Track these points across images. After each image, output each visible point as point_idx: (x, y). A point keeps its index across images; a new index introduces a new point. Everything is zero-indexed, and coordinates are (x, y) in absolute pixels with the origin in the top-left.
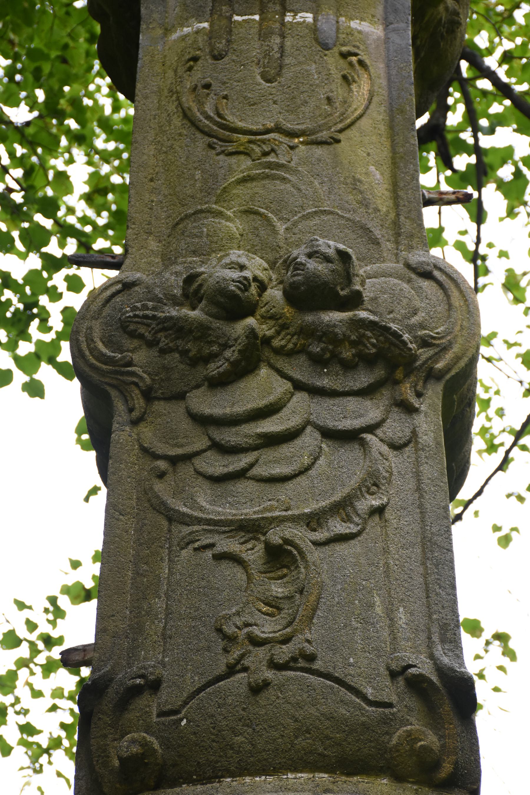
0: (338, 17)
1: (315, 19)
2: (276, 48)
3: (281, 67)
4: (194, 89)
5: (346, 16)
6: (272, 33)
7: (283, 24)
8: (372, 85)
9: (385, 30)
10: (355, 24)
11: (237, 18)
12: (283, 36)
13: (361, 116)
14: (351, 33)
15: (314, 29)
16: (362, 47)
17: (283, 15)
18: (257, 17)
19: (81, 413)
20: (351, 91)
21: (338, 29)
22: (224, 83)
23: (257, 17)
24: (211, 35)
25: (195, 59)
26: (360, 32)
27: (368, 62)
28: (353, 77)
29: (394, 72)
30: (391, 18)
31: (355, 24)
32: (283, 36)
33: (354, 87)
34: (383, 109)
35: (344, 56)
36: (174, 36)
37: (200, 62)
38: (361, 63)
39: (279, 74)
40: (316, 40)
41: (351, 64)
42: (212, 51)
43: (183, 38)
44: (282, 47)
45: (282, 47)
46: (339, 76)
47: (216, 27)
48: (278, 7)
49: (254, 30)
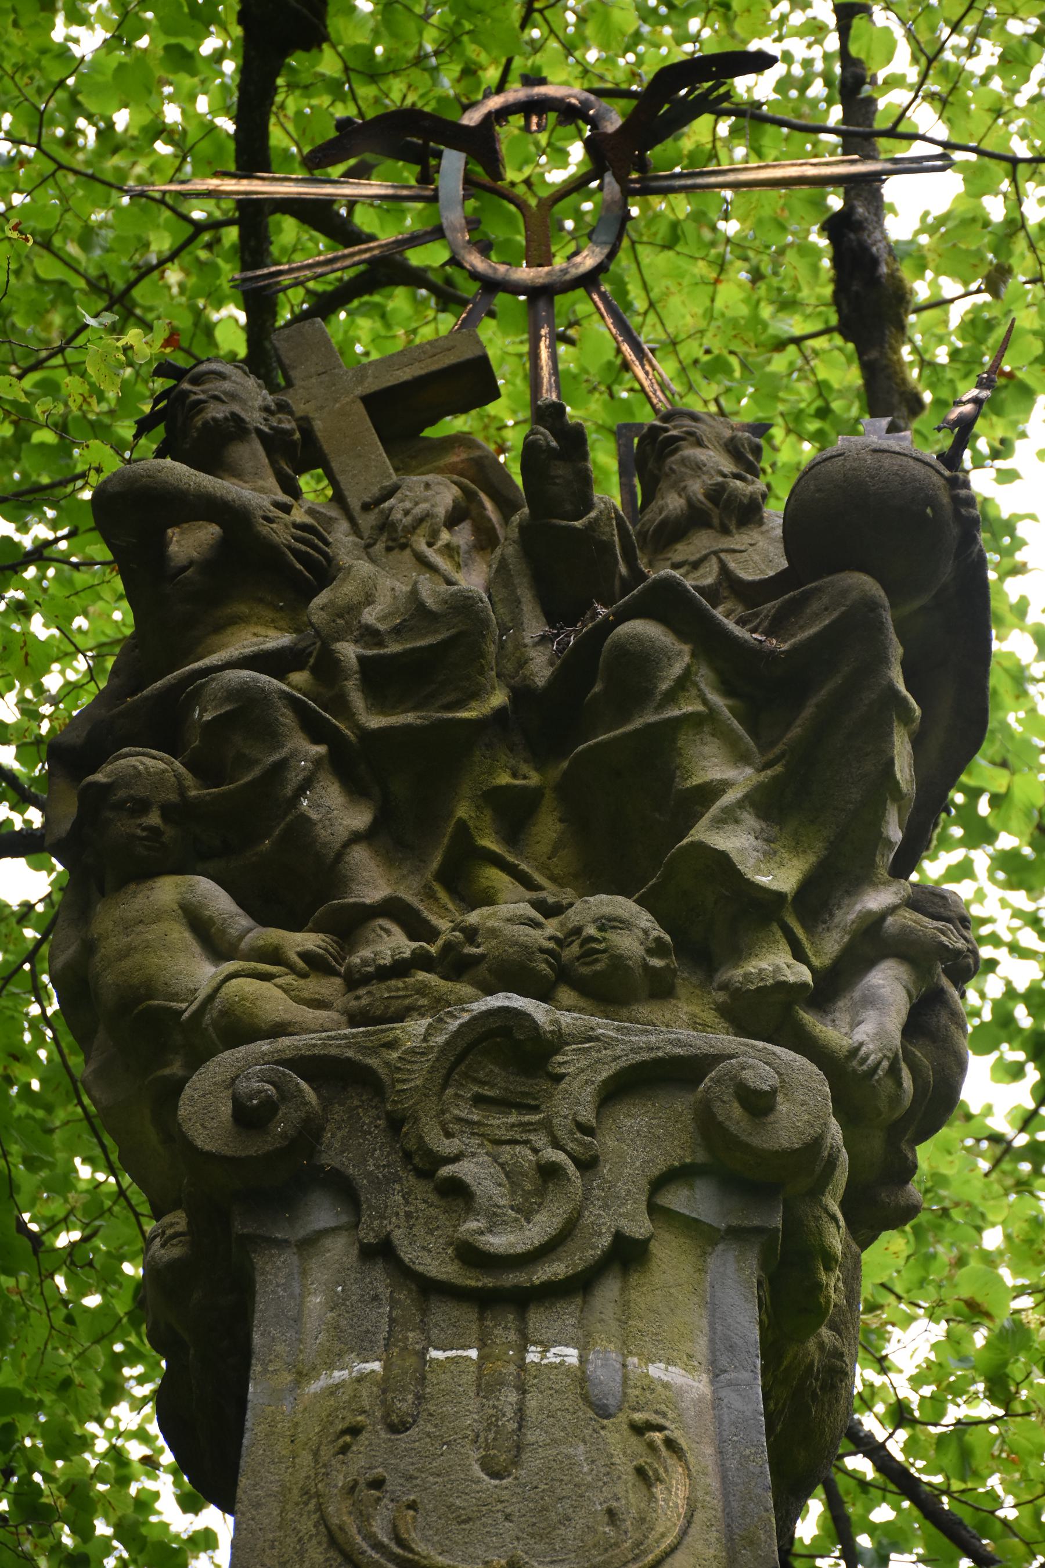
1: (582, 1359)
2: (510, 1414)
3: (519, 1448)
5: (640, 1355)
6: (502, 1384)
7: (522, 1366)
8: (693, 1488)
9: (712, 1382)
10: (656, 1370)
11: (434, 1354)
12: (522, 1390)
13: (673, 1549)
14: (649, 1386)
15: (581, 1378)
16: (671, 1415)
18: (473, 1353)
20: (652, 1497)
21: (625, 1378)
23: (473, 1353)
24: (386, 1384)
25: (355, 1431)
26: (666, 1386)
27: (683, 1443)
28: (655, 1471)
29: (732, 1464)
30: (724, 1361)
31: (656, 1370)
32: (522, 1390)
33: (658, 1490)
34: (713, 1535)
35: (639, 1429)
36: (315, 1387)
37: (363, 1437)
38: (670, 1443)
39: (516, 1462)
40: (585, 1398)
41: (651, 1446)
42: (387, 1415)
44: (520, 1411)
45: (520, 1411)
46: (630, 1469)
48: (513, 1336)
49: (469, 1378)
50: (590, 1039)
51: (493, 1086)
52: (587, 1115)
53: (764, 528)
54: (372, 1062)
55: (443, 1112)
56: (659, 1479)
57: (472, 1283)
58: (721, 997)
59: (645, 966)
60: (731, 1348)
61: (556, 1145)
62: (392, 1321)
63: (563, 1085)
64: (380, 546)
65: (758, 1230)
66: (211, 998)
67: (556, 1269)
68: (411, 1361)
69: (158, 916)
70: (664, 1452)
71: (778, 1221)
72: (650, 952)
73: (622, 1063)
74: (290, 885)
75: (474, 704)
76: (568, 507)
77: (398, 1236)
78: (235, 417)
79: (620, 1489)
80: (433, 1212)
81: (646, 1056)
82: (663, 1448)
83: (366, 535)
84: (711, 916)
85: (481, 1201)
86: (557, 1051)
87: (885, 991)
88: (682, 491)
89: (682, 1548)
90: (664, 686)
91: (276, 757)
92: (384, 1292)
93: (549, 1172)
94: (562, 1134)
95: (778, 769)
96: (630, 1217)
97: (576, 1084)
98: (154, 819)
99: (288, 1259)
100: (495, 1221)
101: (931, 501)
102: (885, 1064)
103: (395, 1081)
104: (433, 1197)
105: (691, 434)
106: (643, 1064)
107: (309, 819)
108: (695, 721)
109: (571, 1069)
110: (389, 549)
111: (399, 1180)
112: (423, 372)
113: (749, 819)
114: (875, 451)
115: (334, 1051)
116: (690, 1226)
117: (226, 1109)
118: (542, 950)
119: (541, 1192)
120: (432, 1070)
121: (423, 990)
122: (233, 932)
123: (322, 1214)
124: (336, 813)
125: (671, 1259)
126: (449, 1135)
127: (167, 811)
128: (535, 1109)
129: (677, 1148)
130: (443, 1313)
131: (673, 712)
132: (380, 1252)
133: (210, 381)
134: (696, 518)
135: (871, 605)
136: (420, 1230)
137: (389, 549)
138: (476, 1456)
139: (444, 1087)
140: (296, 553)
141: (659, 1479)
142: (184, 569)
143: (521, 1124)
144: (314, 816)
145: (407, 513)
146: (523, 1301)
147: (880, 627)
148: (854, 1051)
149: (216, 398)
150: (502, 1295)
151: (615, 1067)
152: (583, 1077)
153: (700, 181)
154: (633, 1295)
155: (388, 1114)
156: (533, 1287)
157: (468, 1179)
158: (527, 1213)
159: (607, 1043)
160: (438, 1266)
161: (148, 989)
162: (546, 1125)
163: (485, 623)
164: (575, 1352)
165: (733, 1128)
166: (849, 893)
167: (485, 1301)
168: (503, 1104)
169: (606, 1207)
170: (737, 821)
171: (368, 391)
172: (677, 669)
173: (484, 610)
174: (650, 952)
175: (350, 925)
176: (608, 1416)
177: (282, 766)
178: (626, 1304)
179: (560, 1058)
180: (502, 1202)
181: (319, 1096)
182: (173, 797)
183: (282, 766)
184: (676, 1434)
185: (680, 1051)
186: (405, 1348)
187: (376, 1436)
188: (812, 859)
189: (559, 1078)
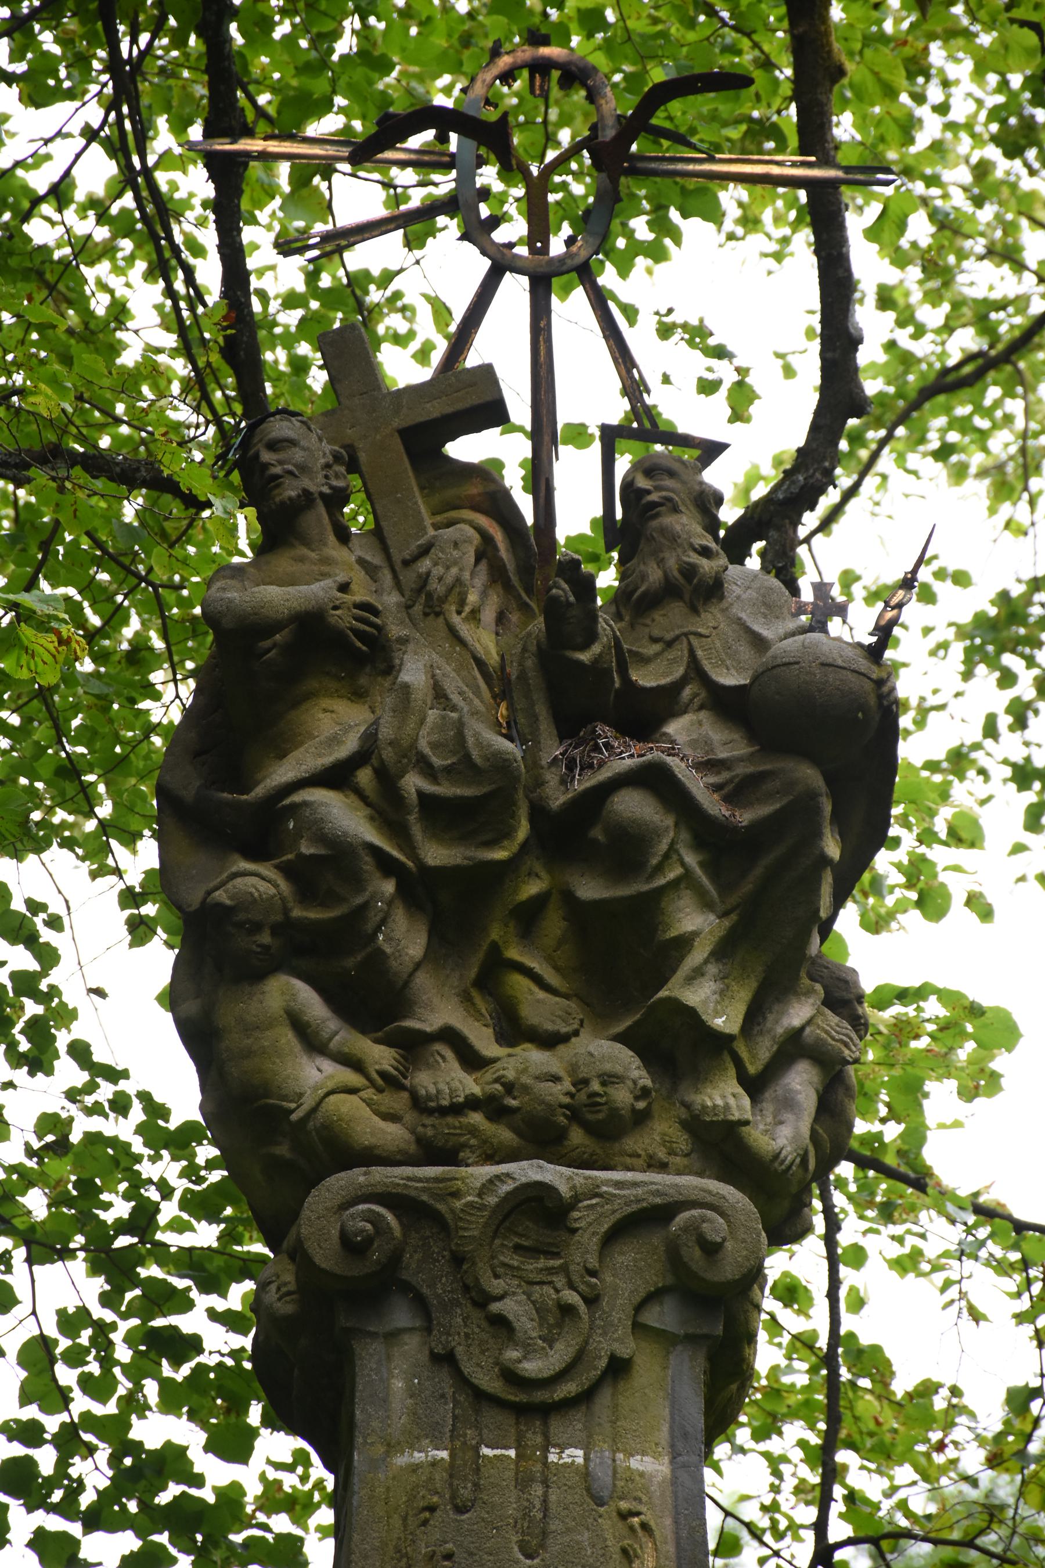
0: (614, 1452)
1: (587, 1458)
3: (545, 1534)
5: (624, 1451)
6: (532, 1480)
11: (486, 1451)
12: (546, 1483)
14: (631, 1476)
15: (586, 1473)
16: (644, 1498)
17: (546, 1451)
18: (512, 1453)
19: (168, 980)
21: (615, 1472)
22: (471, 1554)
23: (512, 1453)
24: (452, 1469)
25: (432, 1509)
26: (642, 1475)
27: (652, 1523)
29: (684, 1534)
30: (680, 1445)
32: (546, 1483)
35: (624, 1516)
36: (401, 1460)
37: (438, 1513)
38: (644, 1526)
39: (542, 1546)
40: (588, 1490)
41: (632, 1528)
42: (453, 1497)
43: (415, 1468)
44: (545, 1501)
45: (545, 1501)
47: (459, 1462)
48: (539, 1439)
49: (510, 1474)
51: (528, 1238)
52: (593, 1262)
53: (724, 604)
54: (441, 1207)
55: (493, 1258)
56: (637, 1557)
57: (512, 1398)
58: (683, 1114)
59: (633, 1110)
60: (685, 1435)
61: (572, 1286)
62: (455, 1417)
63: (577, 1237)
64: (418, 608)
65: (706, 1337)
66: (314, 1110)
68: (470, 1454)
70: (640, 1532)
71: (719, 1330)
72: (637, 1098)
73: (618, 1216)
74: (371, 1000)
75: (506, 843)
77: (460, 1350)
80: (484, 1336)
81: (635, 1207)
83: (408, 593)
84: (679, 1048)
87: (801, 1098)
88: (661, 562)
90: (654, 861)
91: (359, 900)
92: (449, 1391)
93: (567, 1310)
94: (576, 1278)
95: (734, 917)
97: (586, 1236)
98: (266, 938)
99: (376, 1347)
103: (458, 1228)
104: (484, 1324)
105: (669, 500)
106: (633, 1214)
107: (383, 952)
108: (675, 884)
109: (582, 1224)
110: (426, 615)
111: (459, 1305)
112: (449, 410)
113: (712, 969)
114: (823, 664)
115: (413, 1193)
118: (561, 1106)
119: (559, 1325)
120: (486, 1225)
121: (473, 1131)
122: (325, 1035)
123: (401, 1316)
124: (406, 940)
125: (647, 1368)
126: (497, 1276)
127: (276, 930)
128: (556, 1255)
129: (654, 1278)
130: (492, 1417)
131: (661, 881)
132: (445, 1359)
133: (283, 449)
134: (669, 591)
135: (812, 796)
138: (514, 1539)
139: (494, 1238)
140: (357, 633)
141: (637, 1557)
144: (388, 950)
145: (440, 579)
146: (546, 1411)
147: (818, 810)
148: (777, 1156)
149: (290, 473)
150: (534, 1409)
151: (613, 1219)
152: (591, 1230)
153: (680, 166)
155: (451, 1251)
157: (511, 1317)
158: (550, 1341)
160: (489, 1382)
161: (265, 1089)
162: (564, 1269)
163: (517, 779)
164: (580, 1453)
165: (694, 1267)
166: (778, 1000)
167: (521, 1411)
168: (534, 1252)
169: (605, 1334)
171: (405, 424)
172: (664, 846)
173: (518, 768)
174: (637, 1098)
175: (413, 1047)
176: (602, 1505)
177: (364, 907)
178: (616, 1406)
179: (576, 1214)
180: (534, 1334)
181: (401, 1223)
182: (279, 918)
184: (648, 1517)
185: (658, 1200)
186: (465, 1443)
187: (446, 1514)
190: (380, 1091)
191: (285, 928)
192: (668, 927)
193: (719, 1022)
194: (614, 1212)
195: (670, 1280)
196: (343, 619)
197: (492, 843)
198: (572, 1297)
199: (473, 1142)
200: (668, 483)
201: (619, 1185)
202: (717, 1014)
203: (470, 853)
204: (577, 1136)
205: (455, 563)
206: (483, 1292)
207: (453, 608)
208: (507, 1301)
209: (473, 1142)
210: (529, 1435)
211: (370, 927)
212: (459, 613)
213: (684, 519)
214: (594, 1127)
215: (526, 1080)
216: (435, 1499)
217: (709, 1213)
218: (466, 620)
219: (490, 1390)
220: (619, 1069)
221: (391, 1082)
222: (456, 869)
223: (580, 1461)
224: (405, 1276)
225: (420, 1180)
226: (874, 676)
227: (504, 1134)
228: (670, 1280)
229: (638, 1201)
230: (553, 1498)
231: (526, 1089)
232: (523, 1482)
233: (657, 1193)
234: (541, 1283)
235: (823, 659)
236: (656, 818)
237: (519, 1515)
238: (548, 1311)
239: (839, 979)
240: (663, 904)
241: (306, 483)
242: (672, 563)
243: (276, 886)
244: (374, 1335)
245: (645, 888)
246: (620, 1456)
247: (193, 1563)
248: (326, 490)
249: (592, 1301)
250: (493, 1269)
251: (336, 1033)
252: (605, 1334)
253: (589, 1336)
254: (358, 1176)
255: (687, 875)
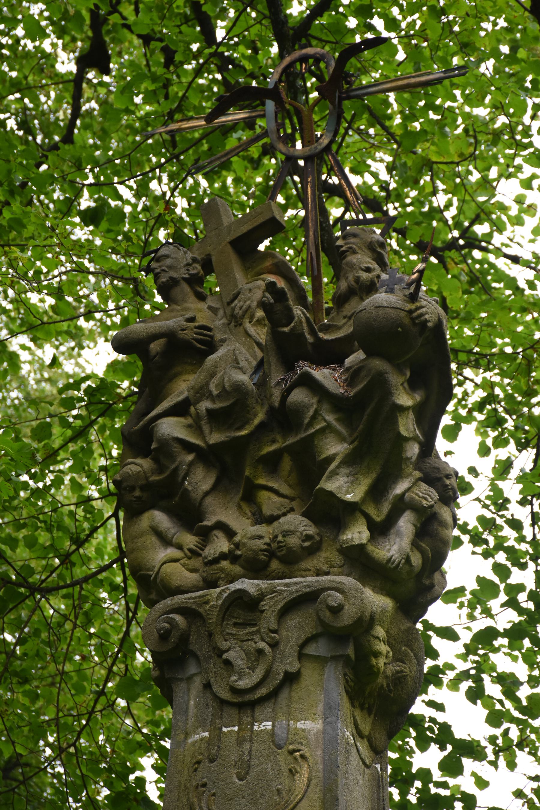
0: (289, 721)
1: (273, 726)
2: (247, 753)
3: (249, 767)
4: (197, 787)
6: (244, 741)
7: (252, 731)
8: (310, 772)
9: (324, 722)
10: (300, 725)
11: (225, 729)
12: (251, 741)
13: (301, 800)
14: (297, 732)
15: (272, 734)
16: (304, 742)
17: (252, 725)
20: (294, 780)
22: (214, 782)
23: (236, 728)
25: (199, 762)
26: (304, 730)
27: (307, 755)
28: (296, 769)
31: (300, 725)
33: (297, 777)
34: (318, 789)
35: (291, 752)
38: (302, 756)
39: (247, 773)
40: (273, 741)
41: (295, 759)
43: (194, 743)
46: (287, 770)
48: (250, 719)
49: (234, 739)
50: (275, 592)
52: (273, 625)
54: (201, 610)
56: (297, 772)
57: (235, 700)
59: (302, 547)
61: (263, 640)
65: (341, 656)
66: (158, 572)
67: (263, 691)
69: (142, 534)
70: (300, 759)
72: (304, 541)
73: (286, 600)
74: (189, 515)
76: (284, 321)
78: (171, 278)
79: (282, 780)
80: (222, 671)
81: (295, 595)
82: (299, 759)
84: (331, 514)
85: (236, 668)
86: (262, 600)
89: (305, 798)
90: (306, 421)
91: (174, 466)
93: (260, 652)
94: (264, 635)
95: (356, 443)
96: (290, 664)
97: (269, 613)
99: (183, 685)
100: (241, 675)
101: (400, 325)
102: (403, 561)
104: (222, 665)
105: (351, 248)
106: (295, 598)
108: (322, 431)
109: (267, 607)
110: (236, 326)
112: (251, 227)
115: (189, 605)
116: (317, 658)
117: (156, 634)
118: (261, 550)
119: (257, 660)
121: (222, 570)
122: (170, 536)
124: (201, 481)
126: (226, 640)
127: (143, 488)
128: (255, 625)
129: (310, 630)
130: (229, 712)
131: (312, 431)
136: (219, 679)
137: (236, 326)
139: (223, 621)
141: (297, 772)
142: (155, 356)
143: (250, 633)
144: (190, 488)
145: (241, 308)
146: (253, 705)
150: (245, 704)
154: (293, 693)
156: (256, 700)
157: (231, 660)
158: (253, 669)
159: (281, 592)
160: (224, 694)
165: (327, 621)
167: (241, 706)
168: (244, 625)
170: (337, 474)
172: (311, 412)
175: (205, 535)
177: (176, 469)
179: (263, 603)
180: (244, 667)
182: (143, 482)
183: (176, 469)
184: (305, 751)
185: (308, 590)
188: (374, 476)
189: (263, 611)
190: (189, 558)
191: (147, 487)
192: (321, 453)
193: (349, 497)
194: (284, 599)
195: (320, 630)
196: (189, 335)
197: (240, 428)
198: (262, 645)
199: (223, 575)
200: (352, 240)
201: (287, 585)
202: (348, 493)
203: (228, 434)
204: (275, 565)
205: (249, 299)
206: (219, 649)
207: (247, 321)
208: (231, 652)
209: (223, 575)
210: (245, 718)
211: (180, 480)
212: (250, 322)
213: (359, 256)
214: (282, 558)
215: (245, 540)
216: (200, 757)
217: (331, 592)
218: (254, 325)
219: (225, 698)
220: (292, 528)
221: (194, 553)
222: (222, 443)
223: (270, 727)
224: (191, 647)
225: (193, 598)
226: (407, 309)
227: (237, 569)
228: (320, 630)
229: (297, 592)
230: (254, 748)
231: (244, 544)
232: (240, 742)
233: (308, 586)
234: (248, 640)
235: (377, 304)
236: (306, 400)
237: (237, 759)
238: (251, 654)
239: (434, 468)
240: (316, 442)
241: (174, 275)
242: (351, 278)
243: (142, 467)
244: (181, 680)
245: (303, 435)
246: (292, 722)
247: (463, 807)
248: (187, 276)
249: (274, 645)
250: (223, 636)
251: (175, 534)
252: (282, 661)
253: (272, 663)
254: (168, 602)
255: (329, 427)
